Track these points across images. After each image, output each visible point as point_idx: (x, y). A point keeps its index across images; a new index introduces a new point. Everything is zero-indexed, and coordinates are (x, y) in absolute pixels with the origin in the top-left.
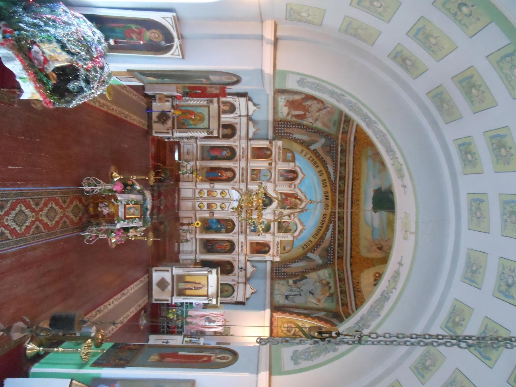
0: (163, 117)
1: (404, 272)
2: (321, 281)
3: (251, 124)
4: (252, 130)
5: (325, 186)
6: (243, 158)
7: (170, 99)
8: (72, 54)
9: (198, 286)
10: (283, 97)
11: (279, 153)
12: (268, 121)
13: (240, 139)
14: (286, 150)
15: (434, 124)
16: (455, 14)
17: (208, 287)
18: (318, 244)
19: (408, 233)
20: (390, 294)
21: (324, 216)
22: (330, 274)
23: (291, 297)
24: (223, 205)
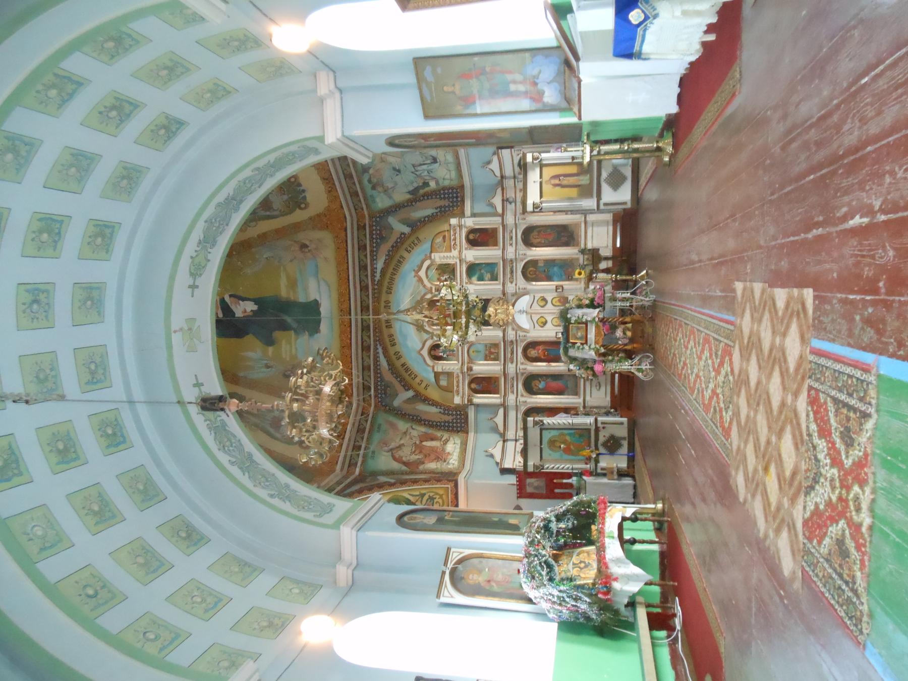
0: (612, 445)
1: (183, 277)
2: (386, 191)
3: (501, 428)
4: (499, 420)
5: (391, 336)
6: (513, 379)
7: (599, 471)
8: (549, 566)
9: (559, 181)
10: (450, 466)
11: (458, 386)
12: (476, 432)
13: (517, 405)
14: (448, 389)
15: (158, 463)
16: (103, 587)
17: (541, 183)
18: (396, 247)
19: (186, 328)
20: (198, 249)
21: (389, 291)
22: (374, 201)
23: (429, 162)
24: (542, 303)
